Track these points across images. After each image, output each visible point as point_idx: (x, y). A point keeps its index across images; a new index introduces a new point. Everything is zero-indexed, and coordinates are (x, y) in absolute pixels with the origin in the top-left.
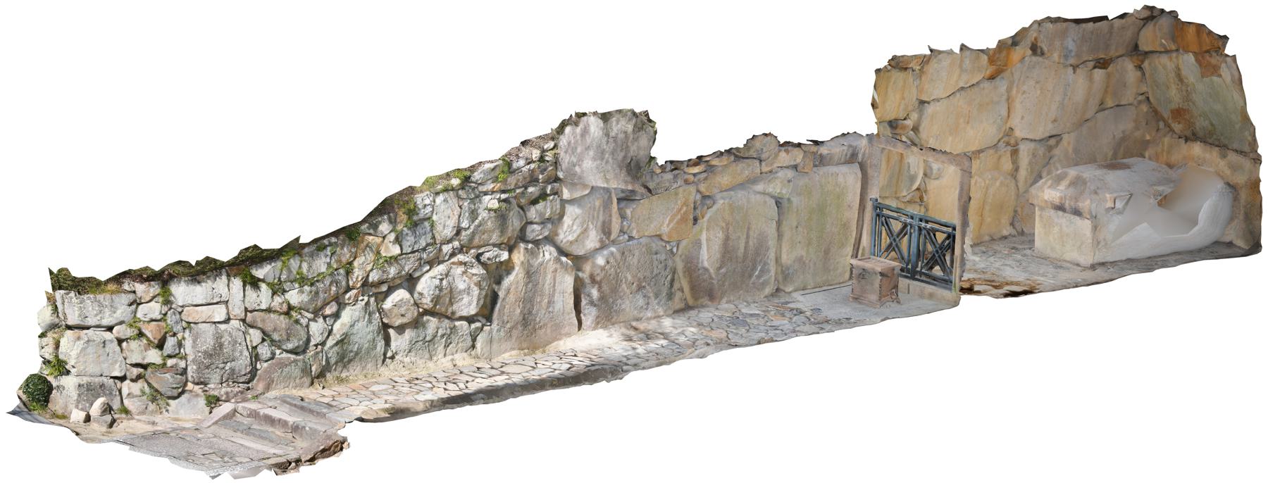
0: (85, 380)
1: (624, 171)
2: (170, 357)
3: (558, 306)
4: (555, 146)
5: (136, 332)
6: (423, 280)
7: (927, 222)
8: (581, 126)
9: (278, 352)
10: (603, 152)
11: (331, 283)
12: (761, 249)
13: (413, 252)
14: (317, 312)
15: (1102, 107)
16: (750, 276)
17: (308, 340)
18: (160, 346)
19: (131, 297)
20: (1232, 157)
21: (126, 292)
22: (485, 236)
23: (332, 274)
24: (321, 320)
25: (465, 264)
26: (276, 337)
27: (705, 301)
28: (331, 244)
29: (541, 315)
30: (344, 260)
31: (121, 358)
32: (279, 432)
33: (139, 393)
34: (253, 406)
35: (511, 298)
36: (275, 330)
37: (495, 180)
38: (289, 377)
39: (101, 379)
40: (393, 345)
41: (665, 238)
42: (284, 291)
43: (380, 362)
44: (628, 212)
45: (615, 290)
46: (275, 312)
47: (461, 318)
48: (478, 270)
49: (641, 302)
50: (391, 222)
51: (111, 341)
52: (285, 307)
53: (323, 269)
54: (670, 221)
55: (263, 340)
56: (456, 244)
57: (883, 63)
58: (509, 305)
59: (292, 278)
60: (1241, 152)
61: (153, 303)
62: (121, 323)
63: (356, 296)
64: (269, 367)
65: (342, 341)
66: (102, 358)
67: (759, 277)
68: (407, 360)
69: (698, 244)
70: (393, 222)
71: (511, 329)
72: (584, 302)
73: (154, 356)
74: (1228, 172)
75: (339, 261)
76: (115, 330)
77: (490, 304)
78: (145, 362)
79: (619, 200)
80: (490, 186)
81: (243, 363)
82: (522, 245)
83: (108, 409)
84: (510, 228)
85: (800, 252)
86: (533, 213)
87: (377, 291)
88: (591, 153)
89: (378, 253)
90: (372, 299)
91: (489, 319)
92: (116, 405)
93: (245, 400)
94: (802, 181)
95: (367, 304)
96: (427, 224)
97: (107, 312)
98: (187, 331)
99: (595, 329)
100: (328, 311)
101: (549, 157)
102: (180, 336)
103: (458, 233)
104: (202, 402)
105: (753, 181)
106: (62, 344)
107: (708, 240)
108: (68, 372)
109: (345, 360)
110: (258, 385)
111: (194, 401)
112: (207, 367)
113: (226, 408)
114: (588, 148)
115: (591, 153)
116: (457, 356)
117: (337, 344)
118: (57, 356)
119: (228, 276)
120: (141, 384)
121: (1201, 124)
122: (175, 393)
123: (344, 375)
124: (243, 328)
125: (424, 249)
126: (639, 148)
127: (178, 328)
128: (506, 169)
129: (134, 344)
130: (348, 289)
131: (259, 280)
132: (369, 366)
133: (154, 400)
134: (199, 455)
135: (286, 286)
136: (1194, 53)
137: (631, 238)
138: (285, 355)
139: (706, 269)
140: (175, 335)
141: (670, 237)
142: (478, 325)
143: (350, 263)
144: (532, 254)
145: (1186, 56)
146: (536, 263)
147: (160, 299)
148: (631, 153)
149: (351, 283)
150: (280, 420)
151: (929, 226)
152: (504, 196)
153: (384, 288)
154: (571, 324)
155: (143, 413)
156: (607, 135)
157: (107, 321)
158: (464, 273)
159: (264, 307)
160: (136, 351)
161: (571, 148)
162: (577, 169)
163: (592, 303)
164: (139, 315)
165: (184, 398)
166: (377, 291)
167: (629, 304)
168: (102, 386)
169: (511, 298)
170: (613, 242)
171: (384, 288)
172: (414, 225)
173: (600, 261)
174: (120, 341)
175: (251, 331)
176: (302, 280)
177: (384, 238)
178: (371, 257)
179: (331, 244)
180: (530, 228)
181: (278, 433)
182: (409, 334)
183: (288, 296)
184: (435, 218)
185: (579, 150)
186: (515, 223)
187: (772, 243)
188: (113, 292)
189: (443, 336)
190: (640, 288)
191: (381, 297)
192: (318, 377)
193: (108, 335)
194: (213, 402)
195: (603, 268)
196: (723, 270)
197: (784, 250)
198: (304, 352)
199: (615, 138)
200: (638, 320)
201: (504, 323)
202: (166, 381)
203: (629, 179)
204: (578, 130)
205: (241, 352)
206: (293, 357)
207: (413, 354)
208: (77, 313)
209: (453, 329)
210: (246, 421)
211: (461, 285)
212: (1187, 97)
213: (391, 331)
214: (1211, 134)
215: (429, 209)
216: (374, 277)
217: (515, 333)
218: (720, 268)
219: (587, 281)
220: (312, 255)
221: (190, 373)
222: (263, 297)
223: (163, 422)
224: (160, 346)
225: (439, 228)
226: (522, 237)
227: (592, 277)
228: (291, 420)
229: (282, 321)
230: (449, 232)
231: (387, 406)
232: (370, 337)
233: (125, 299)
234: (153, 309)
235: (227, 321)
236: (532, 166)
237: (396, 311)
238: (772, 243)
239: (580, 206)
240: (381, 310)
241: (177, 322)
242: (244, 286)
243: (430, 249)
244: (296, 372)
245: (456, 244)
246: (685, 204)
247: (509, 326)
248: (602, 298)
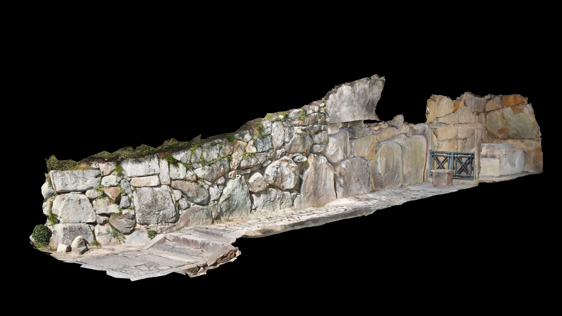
0: (68, 225)
1: (364, 109)
2: (124, 208)
3: (328, 186)
4: (325, 106)
5: (101, 193)
6: (268, 168)
7: (457, 154)
8: (338, 92)
9: (192, 204)
10: (352, 101)
11: (220, 165)
12: (397, 167)
13: (263, 152)
14: (213, 182)
17: (209, 198)
18: (118, 202)
19: (97, 172)
20: (527, 141)
21: (93, 169)
22: (296, 148)
23: (220, 160)
24: (216, 186)
25: (288, 161)
26: (190, 195)
27: (379, 188)
28: (219, 143)
29: (321, 191)
30: (227, 153)
31: (92, 211)
32: (192, 249)
33: (105, 232)
34: (176, 234)
35: (309, 181)
36: (189, 190)
37: (300, 119)
38: (199, 218)
39: (79, 224)
40: (255, 202)
41: (366, 158)
42: (193, 169)
43: (249, 211)
44: (353, 144)
45: (349, 180)
46: (189, 180)
47: (287, 190)
48: (293, 164)
49: (359, 187)
50: (251, 135)
51: (85, 200)
52: (194, 178)
53: (215, 157)
54: (368, 150)
55: (182, 197)
56: (283, 150)
58: (307, 185)
59: (198, 161)
60: (531, 139)
61: (111, 176)
62: (91, 188)
63: (235, 174)
64: (187, 213)
65: (228, 198)
66: (79, 211)
68: (263, 211)
69: (376, 163)
70: (252, 134)
71: (309, 196)
72: (337, 185)
73: (113, 208)
74: (525, 147)
75: (224, 153)
76: (87, 193)
77: (298, 188)
78: (108, 212)
79: (350, 139)
80: (297, 122)
81: (170, 210)
82: (312, 155)
83: (84, 242)
84: (307, 145)
86: (316, 138)
87: (245, 172)
88: (345, 104)
89: (245, 151)
90: (243, 177)
91: (299, 191)
92: (90, 240)
93: (171, 232)
94: (409, 140)
95: (241, 179)
96: (268, 137)
97: (81, 181)
98: (134, 192)
99: (342, 198)
100: (220, 181)
101: (322, 111)
102: (130, 195)
103: (284, 145)
104: (146, 235)
105: (393, 137)
106: (54, 204)
107: (380, 161)
108: (59, 222)
109: (230, 210)
110: (181, 223)
111: (141, 235)
112: (148, 214)
113: (159, 237)
114: (343, 102)
115: (345, 104)
116: (286, 209)
117: (226, 200)
118: (51, 212)
119: (159, 158)
120: (106, 226)
121: (512, 132)
122: (129, 230)
123: (230, 218)
124: (170, 190)
125: (268, 151)
126: (373, 94)
127: (128, 191)
128: (304, 113)
129: (100, 201)
130: (230, 170)
131: (178, 161)
132: (244, 213)
133: (115, 236)
134: (132, 267)
135: (195, 166)
136: (511, 107)
137: (354, 157)
138: (196, 206)
139: (380, 174)
140: (126, 195)
141: (368, 158)
142: (295, 194)
143: (231, 155)
144: (317, 159)
145: (507, 109)
146: (319, 164)
147: (116, 173)
148: (369, 98)
149: (231, 167)
150: (193, 241)
151: (459, 156)
152: (303, 128)
153: (249, 171)
154: (333, 195)
155: (108, 244)
156: (354, 92)
157: (81, 187)
158: (288, 166)
159: (181, 177)
160: (102, 206)
161: (334, 105)
162: (338, 114)
163: (341, 186)
164: (103, 183)
165: (134, 234)
166: (245, 172)
167: (355, 187)
168: (80, 228)
169: (309, 181)
170: (348, 158)
171: (249, 171)
172: (263, 138)
173: (344, 166)
174: (91, 200)
175: (175, 191)
176: (204, 162)
177: (247, 143)
178: (241, 152)
179: (219, 143)
180: (315, 146)
181: (192, 249)
182: (263, 197)
183: (196, 171)
184: (272, 134)
185: (338, 104)
186: (309, 143)
187: (400, 165)
188: (84, 169)
189: (279, 199)
190: (358, 180)
191: (247, 176)
192: (216, 219)
193: (82, 196)
194: (152, 234)
195: (345, 169)
197: (404, 168)
198: (207, 204)
199: (358, 94)
200: (358, 195)
201: (306, 193)
202: (122, 224)
203: (367, 113)
204: (337, 95)
205: (169, 204)
206: (201, 207)
207: (265, 208)
208: (60, 183)
209: (283, 195)
210: (172, 244)
211: (287, 173)
212: (507, 124)
213: (254, 196)
214: (516, 135)
215: (269, 129)
216: (244, 164)
217: (311, 198)
218: (385, 174)
219: (338, 175)
220: (208, 148)
221: (137, 218)
222: (181, 172)
223: (118, 248)
224: (118, 202)
225: (275, 140)
226: (312, 151)
227: (340, 174)
228: (200, 239)
229: (193, 186)
230: (280, 143)
231: (260, 229)
232: (243, 197)
233: (92, 173)
234: (112, 179)
235: (159, 185)
236: (316, 114)
237: (256, 184)
238: (400, 165)
239: (335, 138)
240: (247, 183)
241: (127, 187)
242: (169, 165)
243: (271, 151)
244: (204, 215)
245: (283, 150)
246: (373, 143)
247: (308, 195)
248: (345, 183)
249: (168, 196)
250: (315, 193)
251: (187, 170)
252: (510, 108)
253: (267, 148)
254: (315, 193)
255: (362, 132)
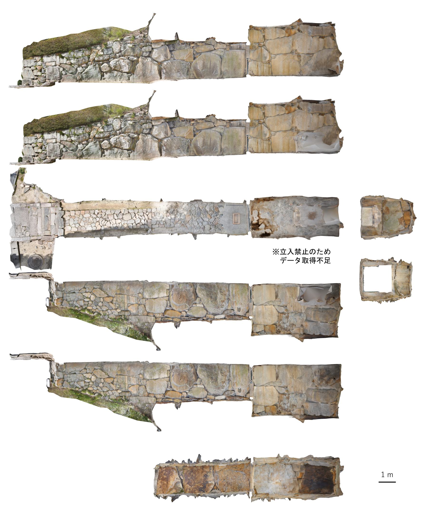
15: (324, 125)
16: (213, 150)
30: (87, 54)
37: (131, 40)
45: (171, 70)
56: (120, 131)
57: (253, 199)
67: (215, 150)
72: (162, 150)
80: (130, 119)
85: (226, 145)
122: (44, 159)
136: (403, 217)
157: (30, 142)
196: (204, 70)
214: (385, 219)
217: (141, 78)
218: (203, 69)
249: (59, 147)
250: (144, 75)
251: (67, 60)
252: (402, 216)
253: (110, 53)
254: (144, 75)
255: (179, 124)
